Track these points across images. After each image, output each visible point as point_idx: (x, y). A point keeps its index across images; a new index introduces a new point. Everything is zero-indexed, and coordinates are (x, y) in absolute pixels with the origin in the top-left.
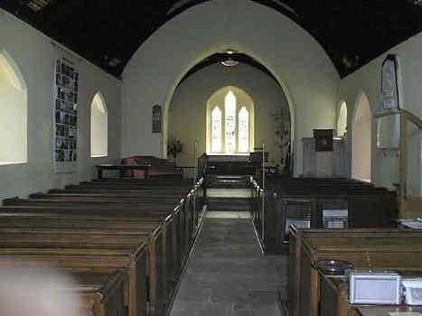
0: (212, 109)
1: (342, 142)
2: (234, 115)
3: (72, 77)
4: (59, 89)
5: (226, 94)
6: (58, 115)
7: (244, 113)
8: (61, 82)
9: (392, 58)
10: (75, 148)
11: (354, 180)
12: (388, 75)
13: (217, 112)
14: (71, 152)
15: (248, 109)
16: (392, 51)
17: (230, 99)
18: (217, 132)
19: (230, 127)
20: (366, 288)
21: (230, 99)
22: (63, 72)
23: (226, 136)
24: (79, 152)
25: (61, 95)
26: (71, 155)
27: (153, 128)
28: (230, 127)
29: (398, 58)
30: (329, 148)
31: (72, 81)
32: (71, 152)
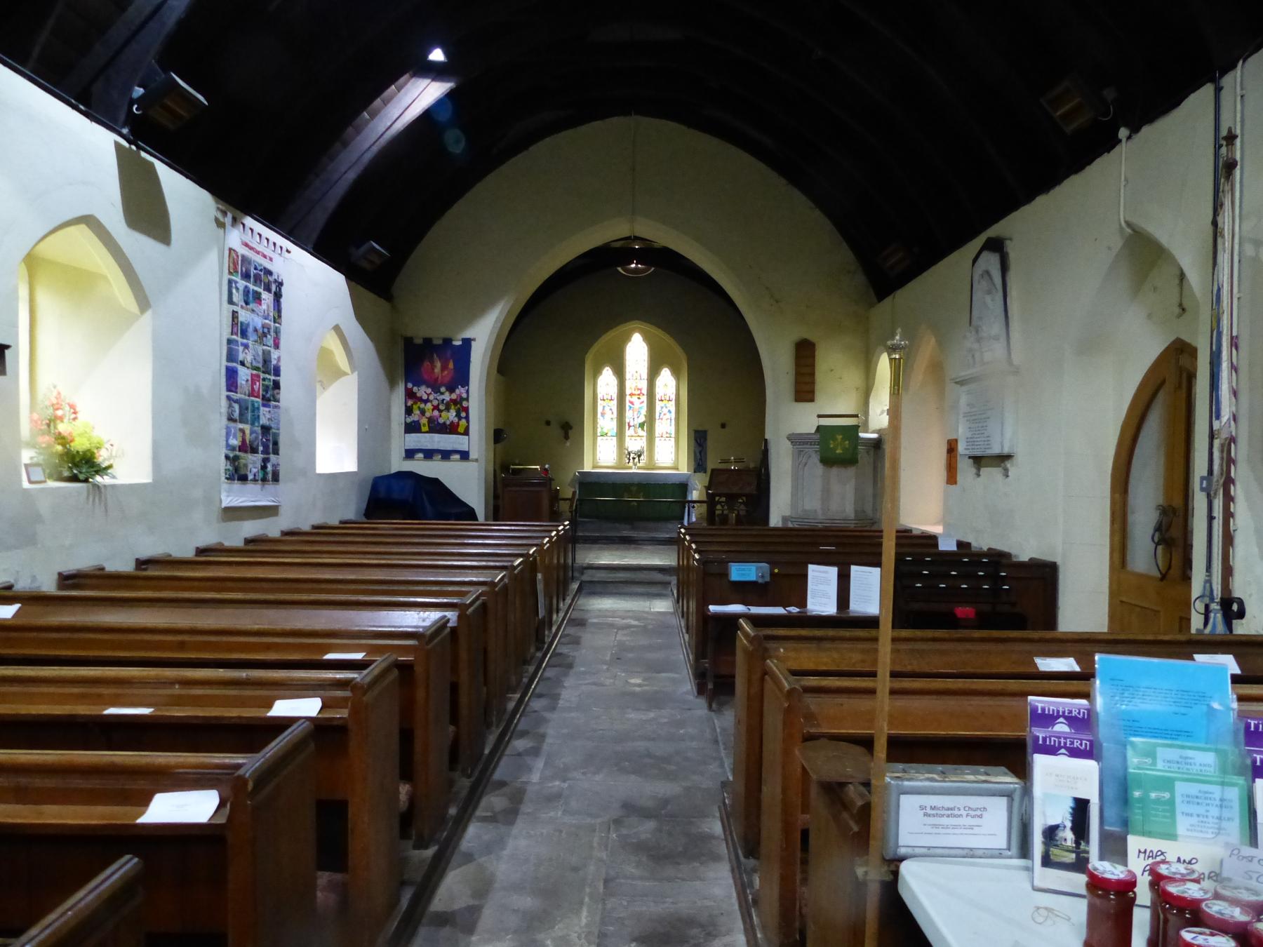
0: (597, 372)
1: (877, 445)
2: (644, 385)
3: (268, 289)
4: (235, 314)
5: (626, 338)
6: (231, 375)
7: (667, 382)
8: (237, 297)
9: (996, 246)
10: (276, 452)
11: (406, 73)
12: (984, 284)
13: (606, 381)
14: (265, 461)
15: (676, 373)
16: (994, 231)
17: (637, 350)
18: (607, 422)
19: (636, 411)
20: (1187, 935)
21: (637, 350)
22: (246, 276)
23: (629, 432)
24: (284, 460)
25: (240, 329)
26: (264, 468)
27: (340, 328)
28: (636, 411)
29: (1012, 249)
30: (848, 461)
31: (267, 298)
32: (265, 461)
